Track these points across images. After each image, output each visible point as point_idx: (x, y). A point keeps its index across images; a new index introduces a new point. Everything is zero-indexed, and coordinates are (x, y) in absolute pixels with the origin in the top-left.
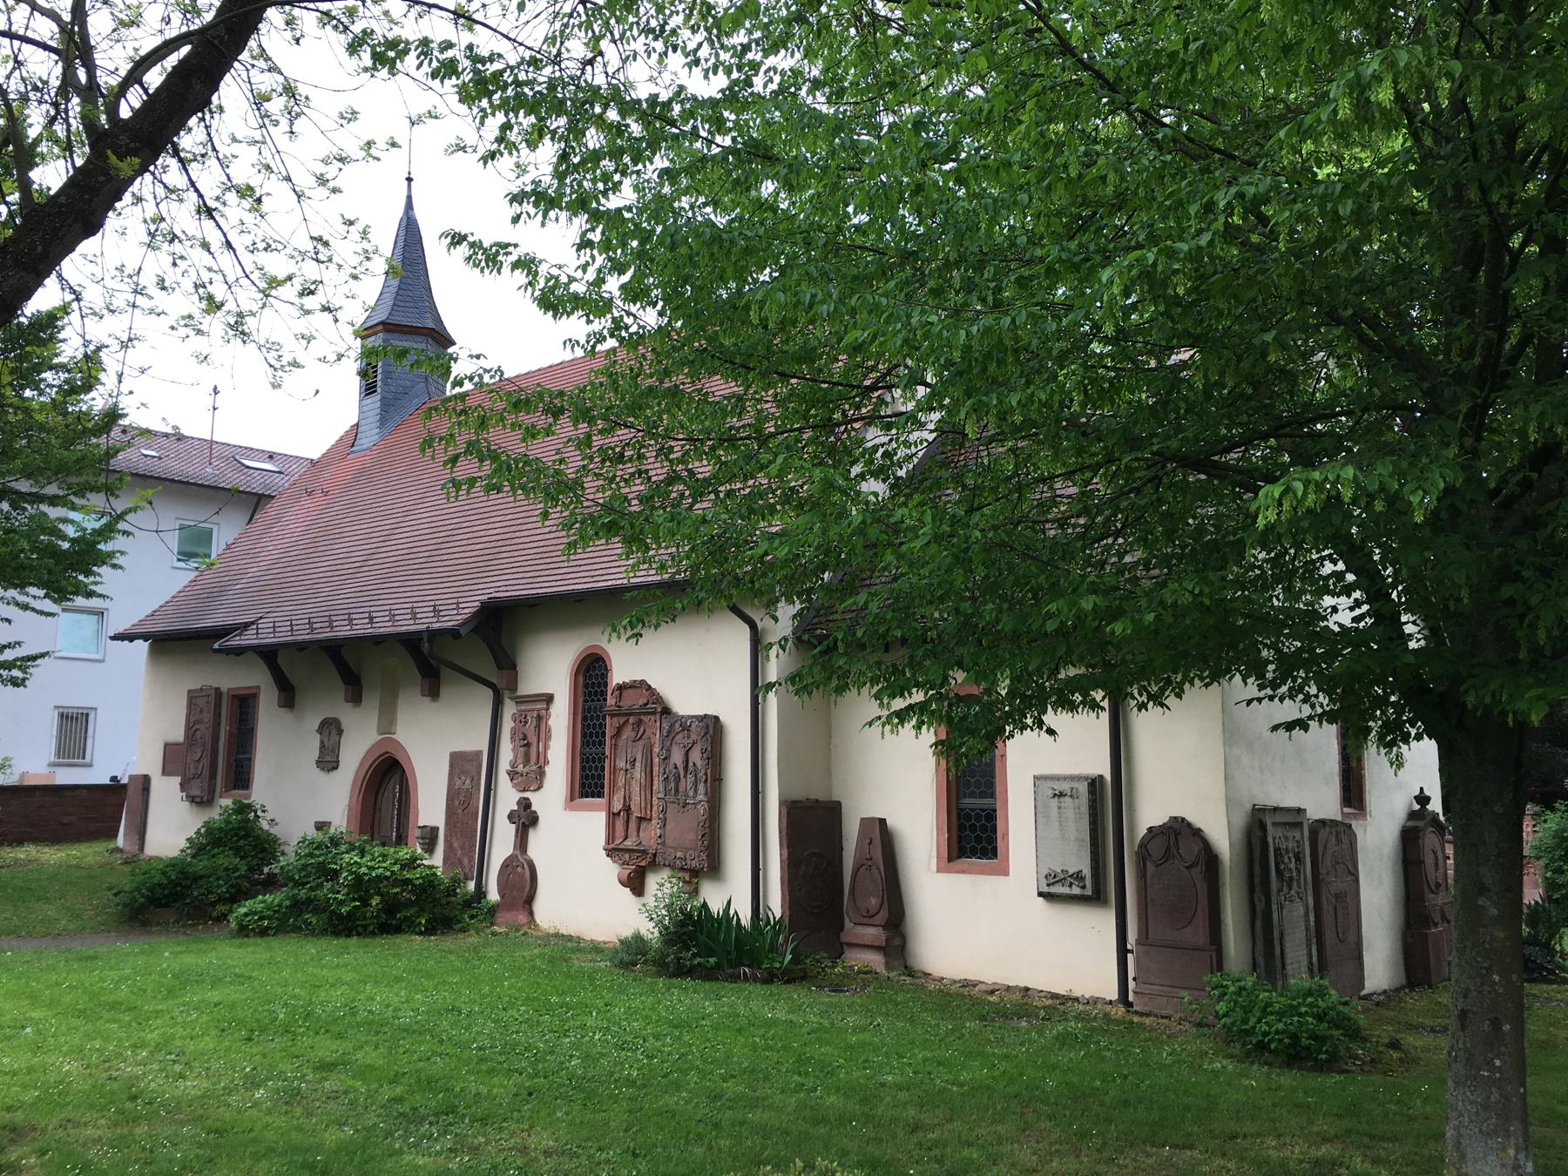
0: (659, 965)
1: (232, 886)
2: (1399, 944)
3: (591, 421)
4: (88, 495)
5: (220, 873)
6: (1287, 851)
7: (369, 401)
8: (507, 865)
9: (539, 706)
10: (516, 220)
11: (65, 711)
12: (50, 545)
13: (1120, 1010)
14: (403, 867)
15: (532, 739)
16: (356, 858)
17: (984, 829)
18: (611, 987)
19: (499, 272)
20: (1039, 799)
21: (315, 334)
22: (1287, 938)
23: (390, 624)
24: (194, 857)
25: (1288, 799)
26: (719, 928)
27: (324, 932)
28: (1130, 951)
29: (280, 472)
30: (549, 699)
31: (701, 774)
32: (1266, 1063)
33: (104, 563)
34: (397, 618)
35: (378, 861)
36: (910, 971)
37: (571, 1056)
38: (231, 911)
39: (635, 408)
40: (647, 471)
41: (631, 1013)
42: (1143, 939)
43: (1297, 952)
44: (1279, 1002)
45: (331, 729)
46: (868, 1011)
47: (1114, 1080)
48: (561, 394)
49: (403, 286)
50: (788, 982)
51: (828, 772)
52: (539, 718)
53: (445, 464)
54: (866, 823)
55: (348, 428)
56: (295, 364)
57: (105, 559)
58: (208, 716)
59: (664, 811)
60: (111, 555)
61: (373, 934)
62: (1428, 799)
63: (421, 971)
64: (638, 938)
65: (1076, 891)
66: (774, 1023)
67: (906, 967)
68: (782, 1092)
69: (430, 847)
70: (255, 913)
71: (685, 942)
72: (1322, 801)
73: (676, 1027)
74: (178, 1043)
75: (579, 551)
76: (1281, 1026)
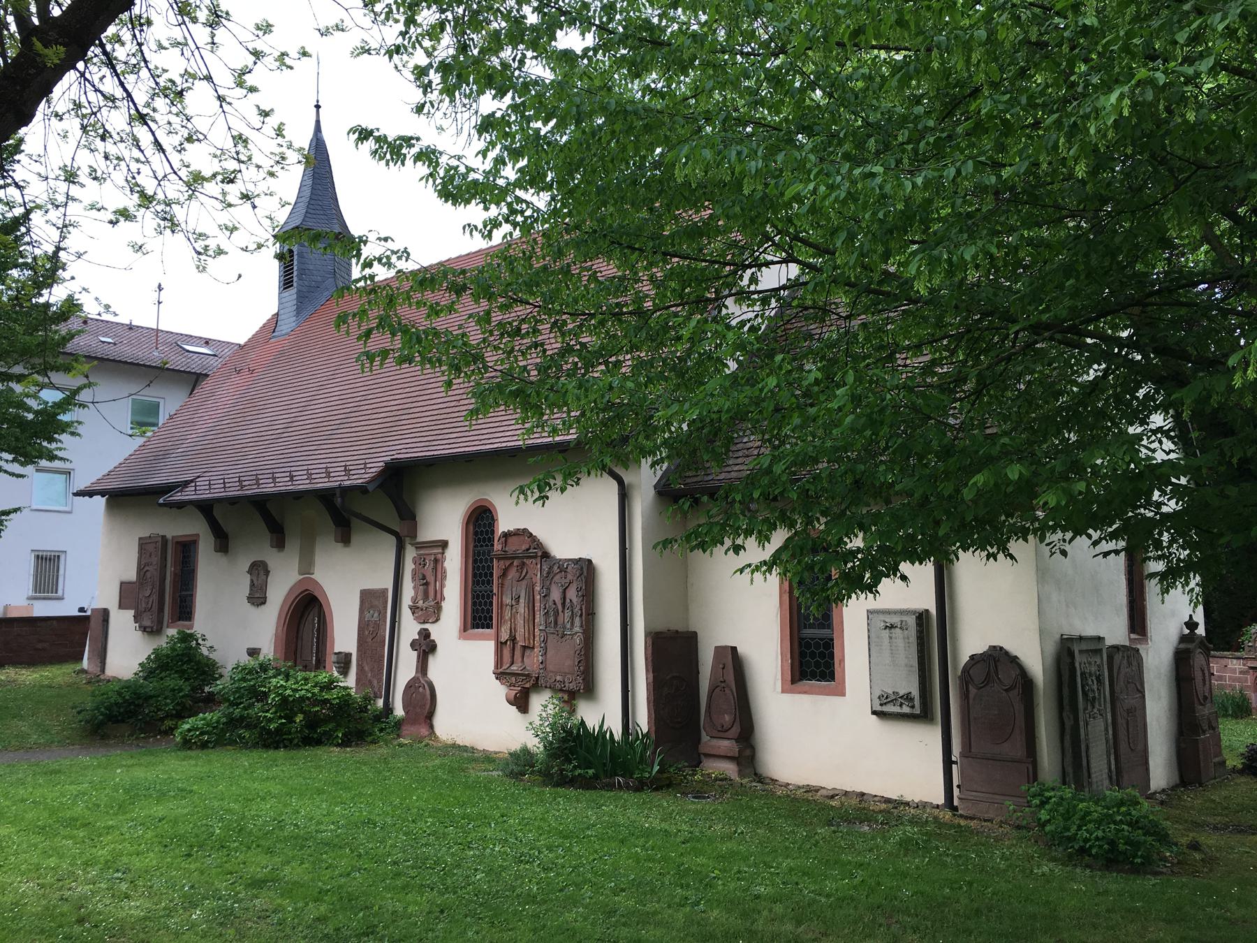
0: (545, 775)
1: (178, 704)
2: (1174, 746)
3: (491, 297)
4: (49, 374)
5: (167, 693)
6: (1091, 675)
7: (287, 294)
8: (410, 686)
9: (435, 551)
10: (419, 109)
11: (40, 554)
12: (17, 416)
13: (947, 815)
14: (322, 689)
15: (430, 578)
16: (282, 682)
17: (822, 655)
18: (505, 797)
19: (403, 164)
20: (872, 630)
21: (237, 225)
22: (1092, 751)
23: (308, 481)
24: (145, 679)
25: (1089, 629)
26: (596, 743)
27: (255, 746)
28: (956, 763)
29: (215, 355)
30: (444, 544)
31: (577, 610)
32: (1087, 866)
33: (63, 431)
34: (314, 476)
35: (300, 684)
36: (760, 778)
37: (476, 870)
38: (176, 727)
39: (530, 285)
40: (542, 345)
41: (524, 823)
42: (967, 752)
43: (1099, 763)
44: (1097, 811)
45: (259, 571)
46: (730, 818)
47: (961, 888)
48: (464, 272)
49: (313, 197)
50: (656, 789)
51: (686, 608)
52: (436, 561)
53: (359, 339)
54: (720, 650)
55: (269, 316)
56: (220, 252)
57: (64, 428)
58: (155, 560)
59: (545, 641)
60: (69, 424)
61: (297, 746)
62: (1196, 625)
63: (339, 782)
64: (525, 751)
65: (906, 710)
66: (648, 834)
67: (756, 774)
68: (669, 906)
69: (344, 671)
70: (197, 729)
71: (566, 755)
72: (1115, 630)
73: (565, 837)
74: (125, 859)
75: (480, 416)
76: (1100, 834)
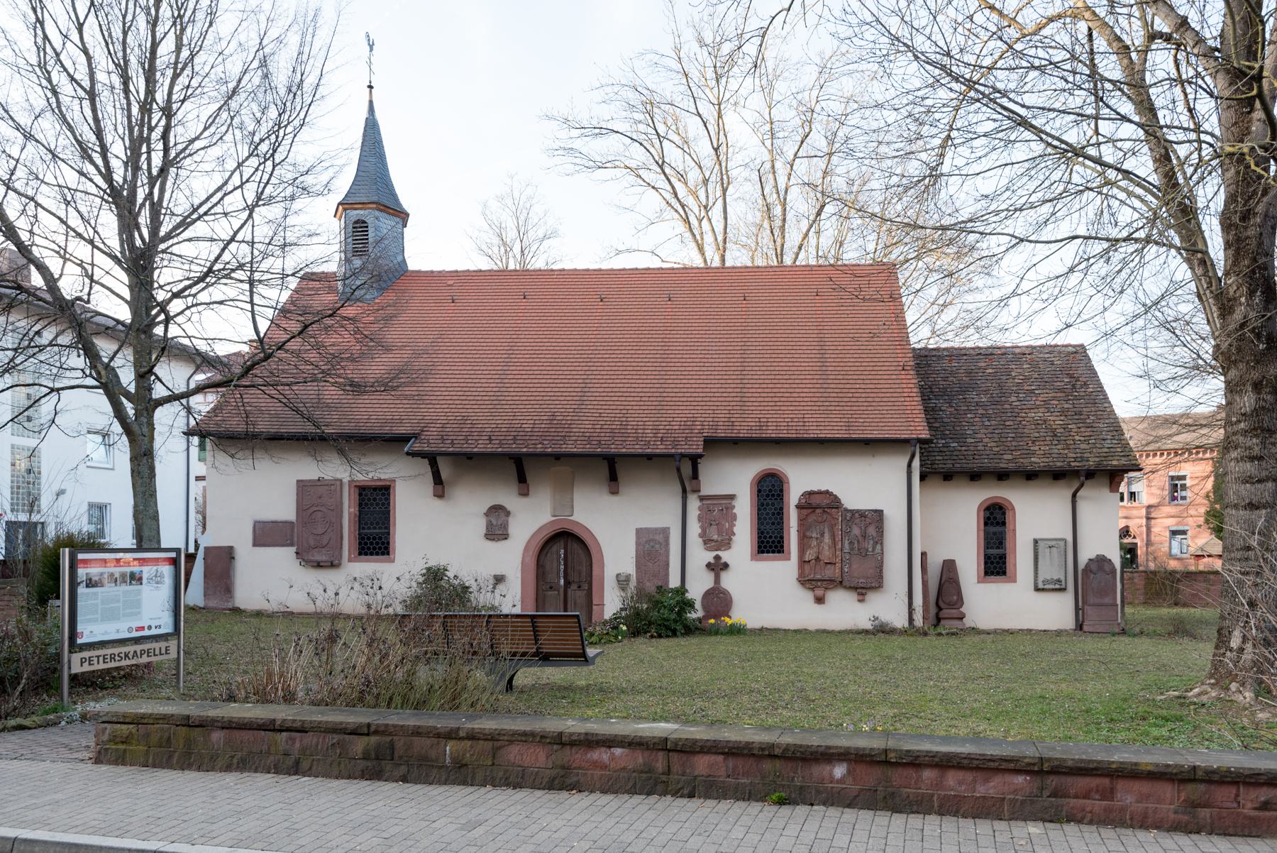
65: (1057, 586)
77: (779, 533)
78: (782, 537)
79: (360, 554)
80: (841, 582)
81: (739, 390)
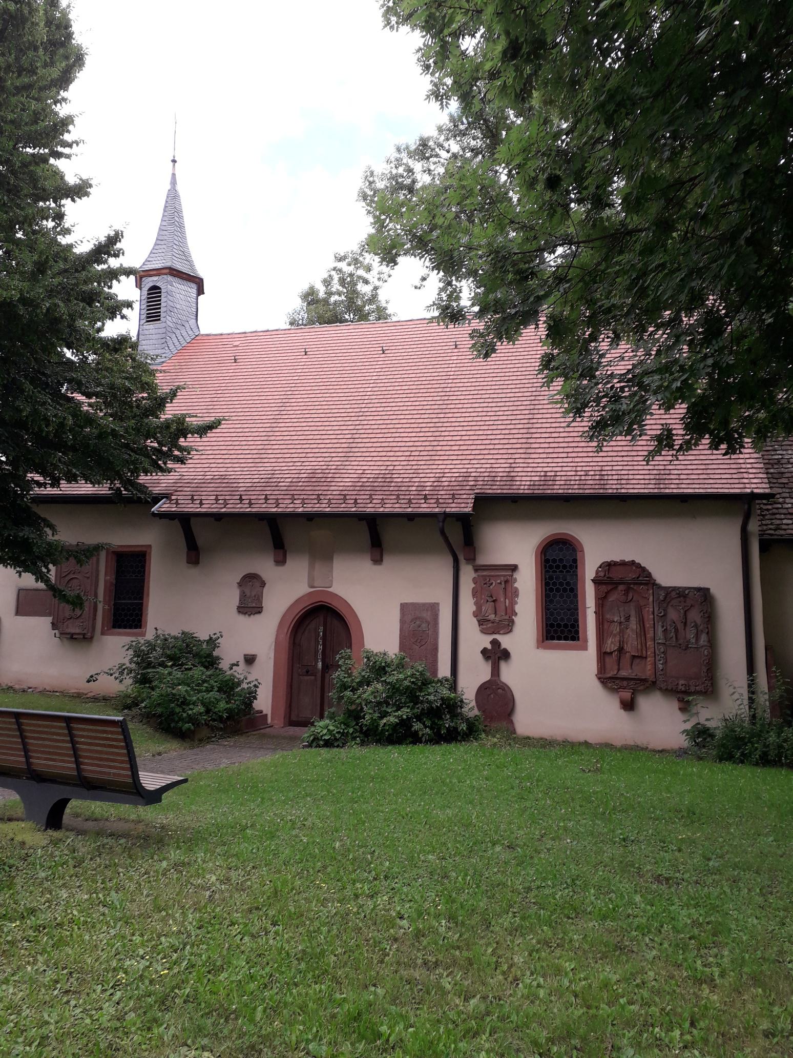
30: (514, 568)
50: (528, 738)
77: (572, 614)
78: (577, 621)
79: (114, 627)
80: (654, 683)
81: (524, 441)
